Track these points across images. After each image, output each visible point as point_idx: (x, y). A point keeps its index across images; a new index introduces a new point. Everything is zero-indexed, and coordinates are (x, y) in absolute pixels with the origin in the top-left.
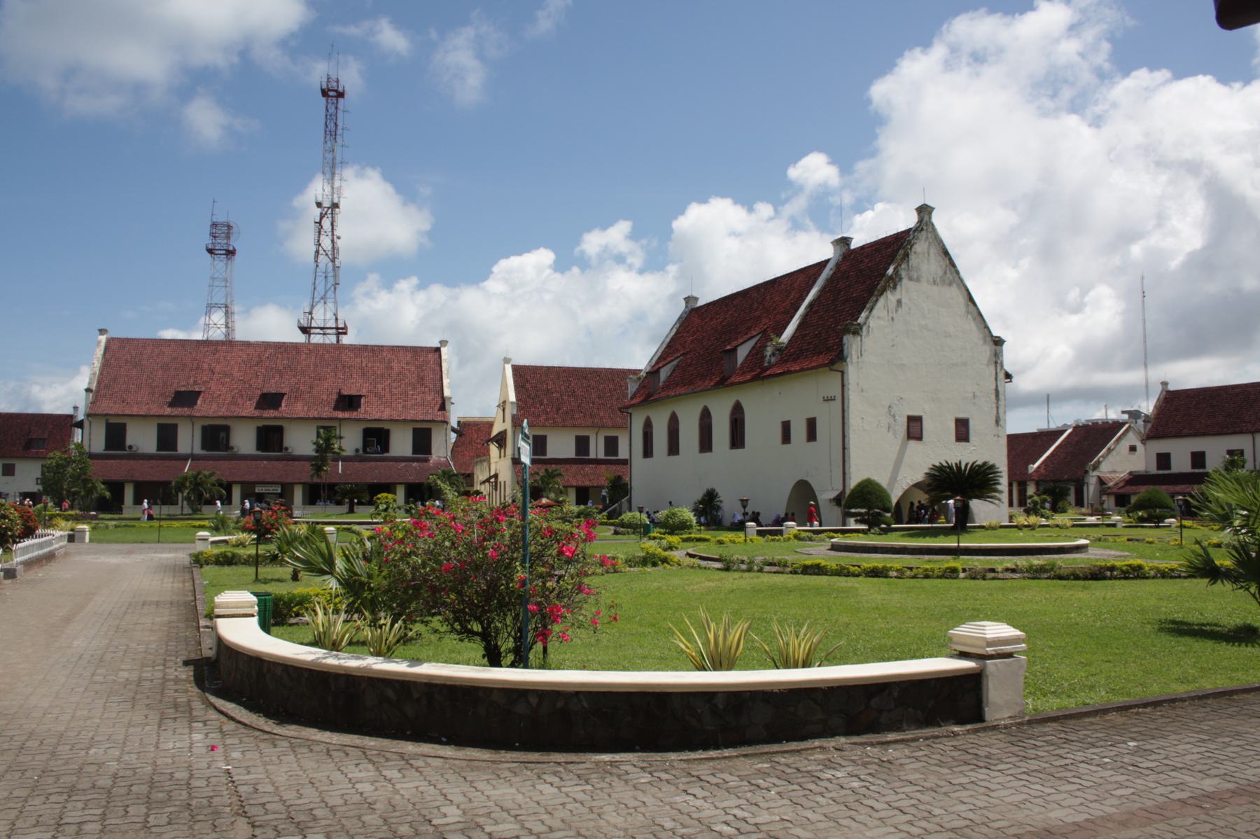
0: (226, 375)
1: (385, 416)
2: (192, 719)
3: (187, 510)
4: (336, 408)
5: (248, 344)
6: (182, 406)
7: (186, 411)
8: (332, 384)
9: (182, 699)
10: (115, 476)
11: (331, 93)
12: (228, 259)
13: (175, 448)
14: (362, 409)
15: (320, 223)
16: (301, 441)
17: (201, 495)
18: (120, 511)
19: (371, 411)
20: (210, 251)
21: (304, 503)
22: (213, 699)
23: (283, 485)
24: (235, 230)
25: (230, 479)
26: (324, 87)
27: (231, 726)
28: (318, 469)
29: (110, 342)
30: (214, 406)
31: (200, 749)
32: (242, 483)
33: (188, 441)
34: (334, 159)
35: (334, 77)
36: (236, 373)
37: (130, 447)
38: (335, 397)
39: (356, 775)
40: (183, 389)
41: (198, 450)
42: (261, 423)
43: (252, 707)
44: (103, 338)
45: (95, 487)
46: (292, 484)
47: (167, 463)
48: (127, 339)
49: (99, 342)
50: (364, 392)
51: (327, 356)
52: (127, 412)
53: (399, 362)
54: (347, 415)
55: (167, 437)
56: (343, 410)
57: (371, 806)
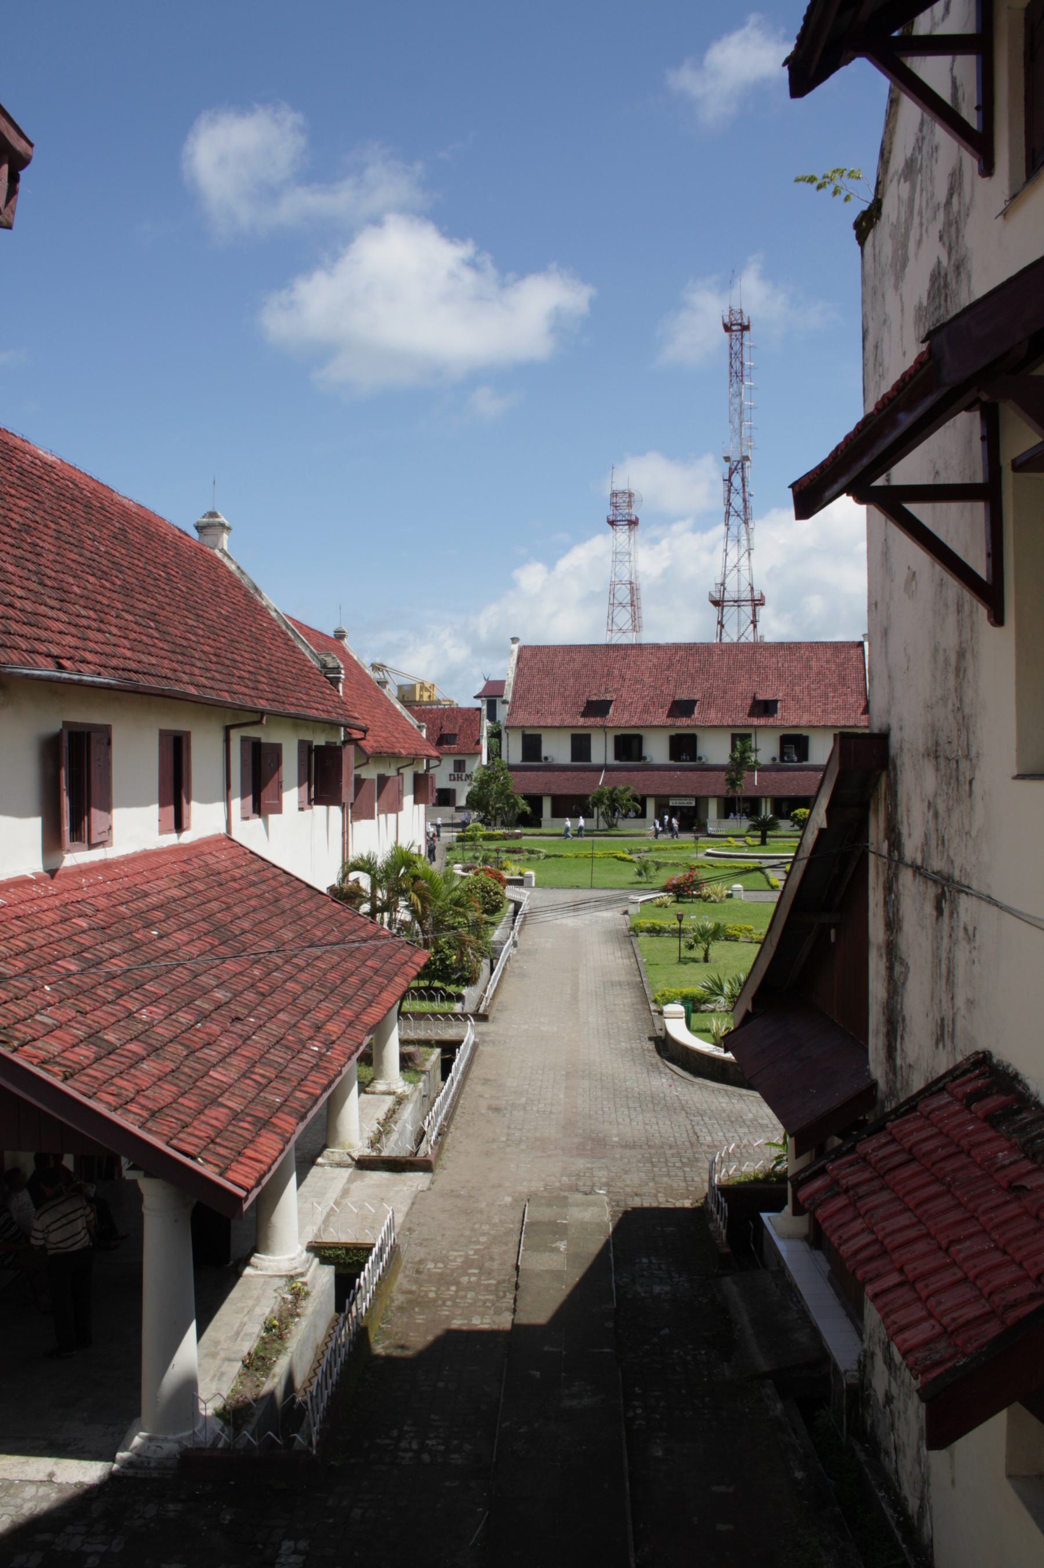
0: (637, 682)
1: (803, 723)
2: (660, 1073)
3: (603, 825)
4: (751, 714)
5: (657, 647)
6: (595, 716)
7: (598, 721)
8: (750, 687)
9: (654, 1062)
10: (534, 791)
11: (734, 328)
12: (630, 530)
13: (588, 758)
14: (779, 715)
15: (729, 480)
16: (716, 750)
17: (618, 808)
18: (539, 825)
19: (788, 717)
20: (612, 523)
21: (718, 817)
22: (667, 1063)
23: (698, 799)
24: (636, 498)
25: (645, 792)
26: (727, 320)
27: (675, 1077)
28: (732, 783)
29: (522, 650)
30: (626, 716)
31: (666, 1085)
32: (657, 797)
33: (602, 751)
34: (741, 404)
35: (736, 308)
36: (647, 679)
37: (546, 758)
38: (749, 702)
39: (721, 1100)
40: (595, 698)
41: (611, 761)
42: (673, 732)
43: (684, 1068)
44: (515, 647)
45: (516, 804)
46: (706, 798)
47: (582, 774)
48: (538, 647)
49: (512, 652)
50: (780, 696)
51: (740, 656)
52: (542, 724)
53: (818, 660)
54: (762, 721)
55: (581, 747)
56: (759, 716)
57: (724, 1111)
